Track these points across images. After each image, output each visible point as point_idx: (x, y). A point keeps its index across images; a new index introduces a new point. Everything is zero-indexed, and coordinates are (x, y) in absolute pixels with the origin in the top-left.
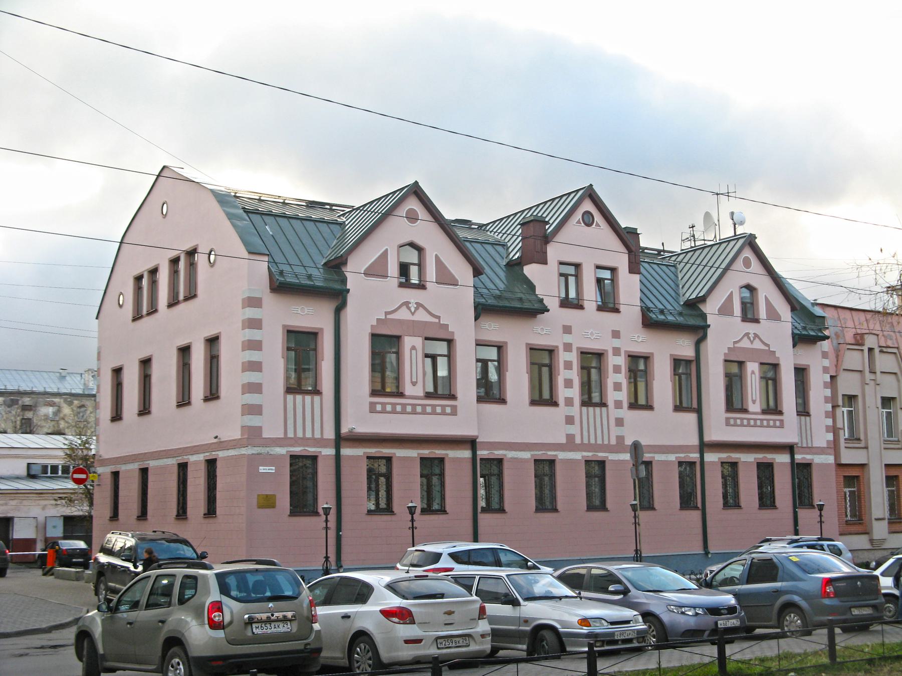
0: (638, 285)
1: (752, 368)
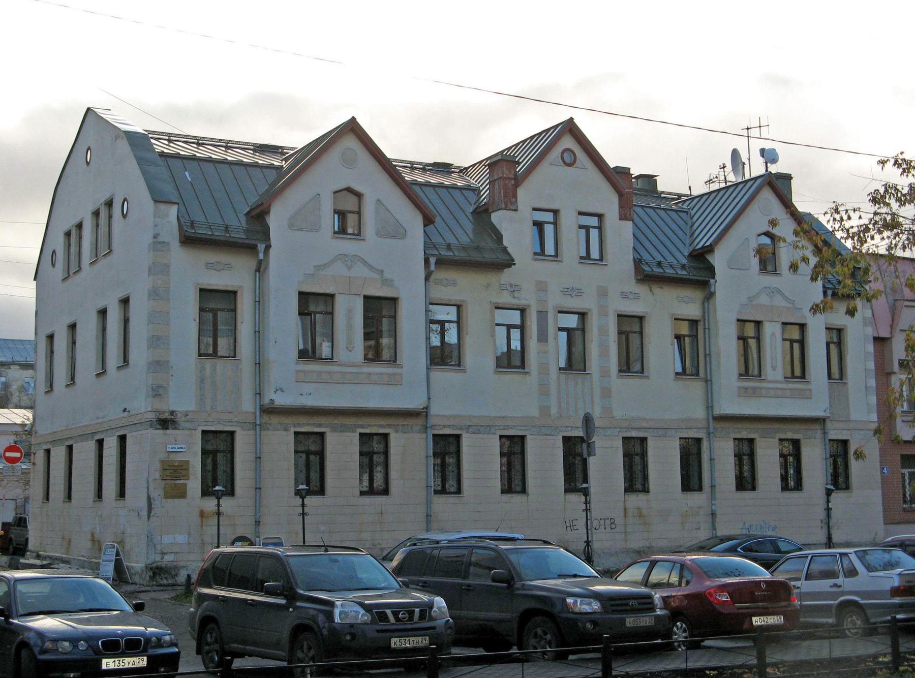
1: (772, 331)
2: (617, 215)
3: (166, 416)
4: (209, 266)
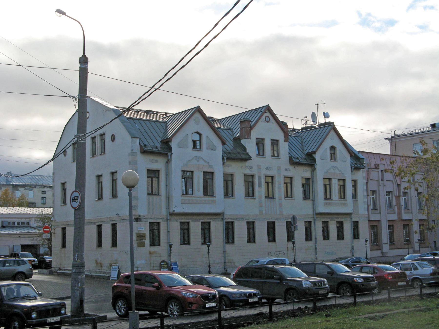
0: (287, 147)
2: (283, 140)
3: (137, 217)
4: (150, 161)
